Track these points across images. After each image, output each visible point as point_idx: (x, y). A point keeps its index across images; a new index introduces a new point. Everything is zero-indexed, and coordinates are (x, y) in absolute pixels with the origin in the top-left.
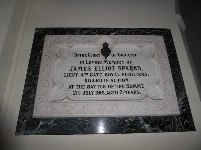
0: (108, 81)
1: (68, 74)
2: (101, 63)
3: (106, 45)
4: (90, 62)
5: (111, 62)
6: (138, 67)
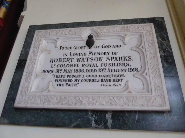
3: (90, 37)
6: (129, 57)
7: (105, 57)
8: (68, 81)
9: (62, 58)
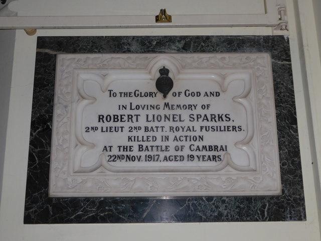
0: (202, 140)
1: (107, 128)
2: (159, 108)
3: (164, 71)
4: (138, 107)
5: (175, 107)
7: (185, 114)
8: (128, 95)
9: (119, 113)
